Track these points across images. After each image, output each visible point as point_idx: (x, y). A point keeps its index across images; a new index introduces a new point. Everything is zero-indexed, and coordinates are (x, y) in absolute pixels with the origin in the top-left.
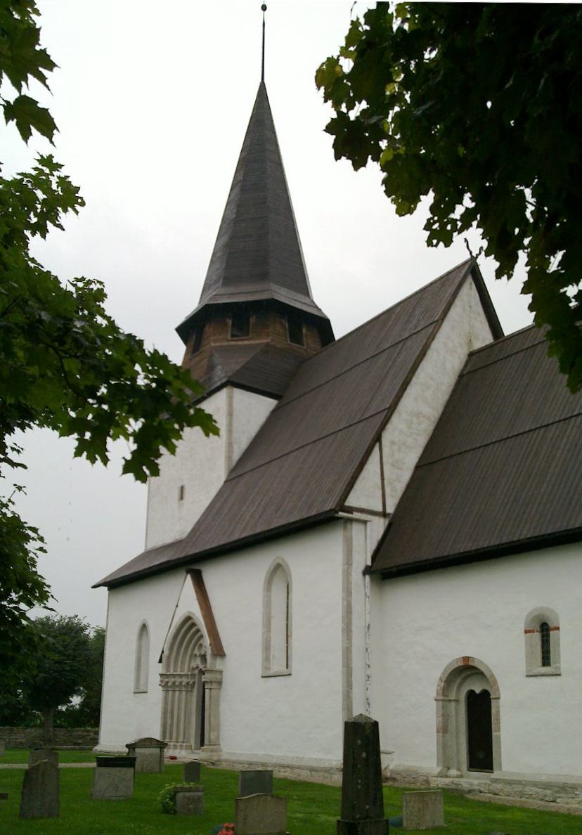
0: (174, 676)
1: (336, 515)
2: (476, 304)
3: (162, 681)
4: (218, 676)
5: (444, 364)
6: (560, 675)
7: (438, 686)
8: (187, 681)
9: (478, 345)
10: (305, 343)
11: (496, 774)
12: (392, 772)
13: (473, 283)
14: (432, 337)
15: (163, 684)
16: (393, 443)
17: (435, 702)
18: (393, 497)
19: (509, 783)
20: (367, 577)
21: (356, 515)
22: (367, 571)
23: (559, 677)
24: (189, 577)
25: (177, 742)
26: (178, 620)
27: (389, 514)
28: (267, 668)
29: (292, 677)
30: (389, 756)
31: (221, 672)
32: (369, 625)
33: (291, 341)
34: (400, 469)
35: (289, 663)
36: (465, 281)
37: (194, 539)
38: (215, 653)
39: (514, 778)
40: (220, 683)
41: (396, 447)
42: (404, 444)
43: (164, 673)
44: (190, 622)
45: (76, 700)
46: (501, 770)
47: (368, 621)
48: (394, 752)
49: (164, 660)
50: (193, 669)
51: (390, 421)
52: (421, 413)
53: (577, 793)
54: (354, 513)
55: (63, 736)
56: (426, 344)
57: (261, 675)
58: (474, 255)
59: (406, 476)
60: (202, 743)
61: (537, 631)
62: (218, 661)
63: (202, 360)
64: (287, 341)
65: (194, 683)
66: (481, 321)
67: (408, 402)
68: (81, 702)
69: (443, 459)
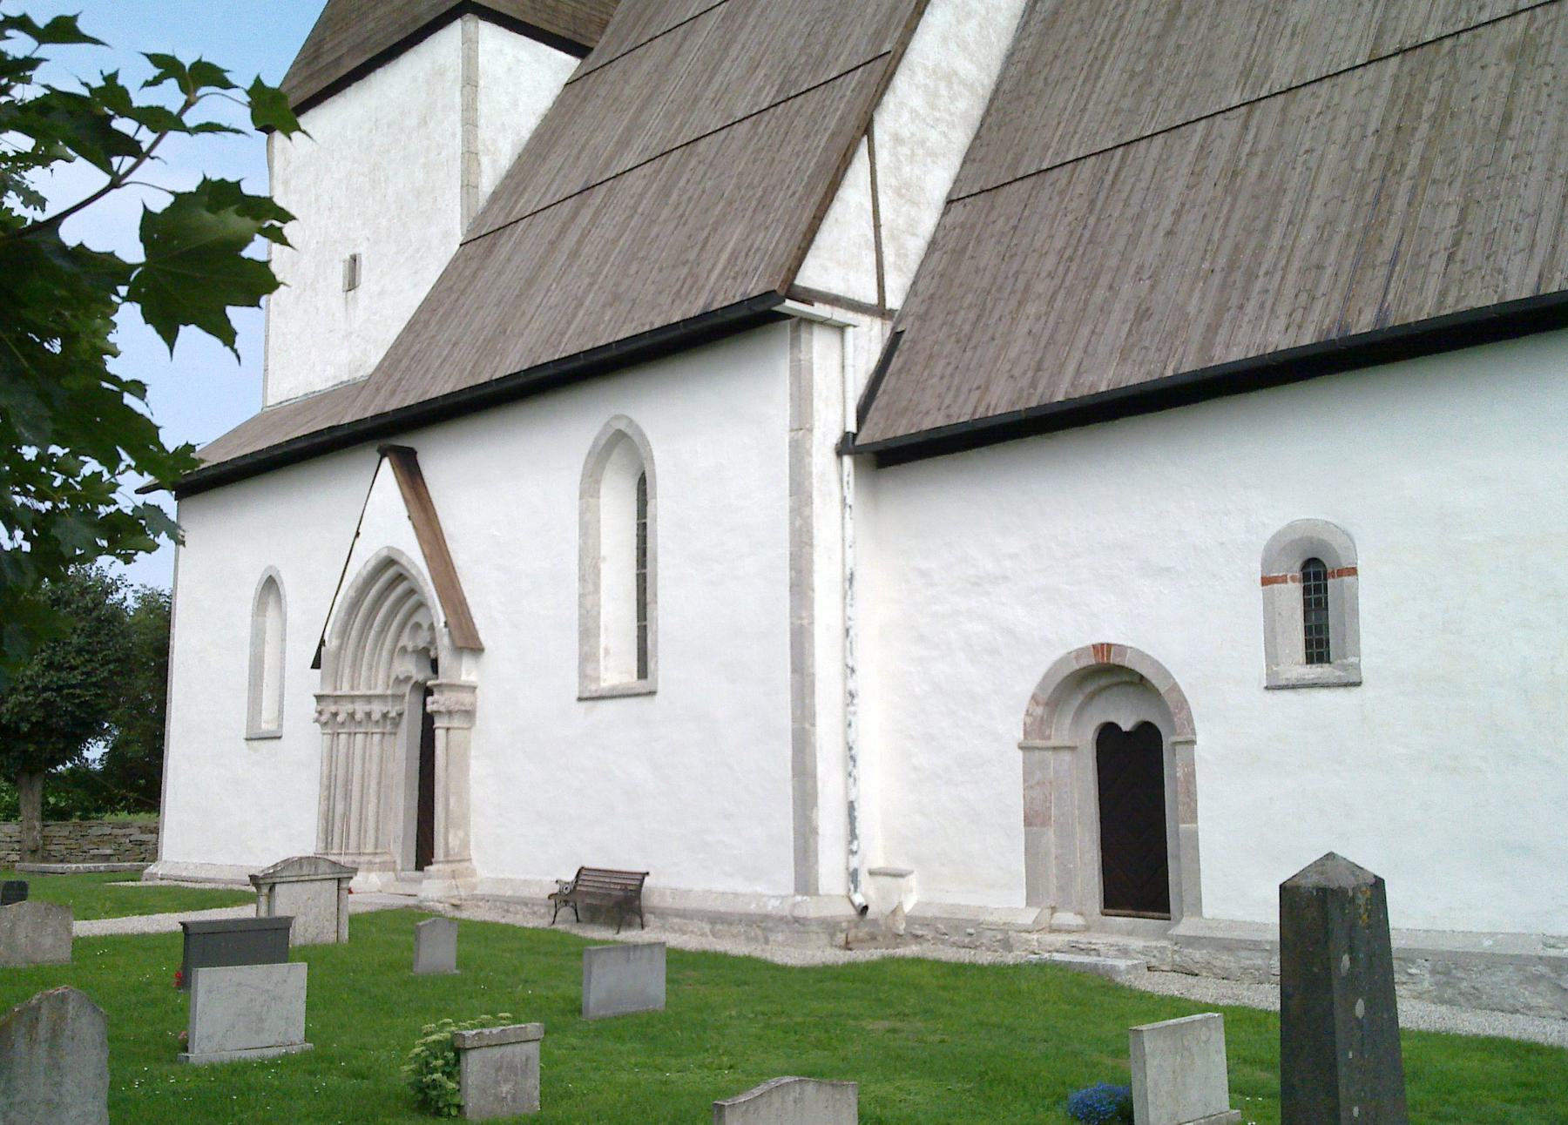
1: (777, 308)
4: (465, 697)
6: (1358, 684)
7: (1028, 714)
11: (1185, 926)
12: (911, 920)
15: (324, 718)
16: (898, 140)
17: (1020, 753)
18: (899, 269)
19: (1228, 946)
20: (847, 460)
21: (820, 310)
22: (846, 446)
23: (1355, 690)
24: (386, 463)
26: (360, 566)
27: (892, 311)
28: (583, 676)
29: (657, 697)
30: (900, 880)
31: (473, 689)
32: (852, 574)
37: (397, 375)
38: (460, 644)
39: (1236, 934)
40: (469, 714)
41: (904, 150)
44: (390, 573)
45: (95, 752)
46: (1200, 913)
47: (849, 564)
48: (911, 873)
50: (398, 681)
51: (891, 86)
52: (956, 73)
53: (1413, 971)
54: (816, 304)
55: (67, 838)
59: (928, 221)
61: (1293, 579)
62: (467, 662)
65: (400, 715)
67: (927, 45)
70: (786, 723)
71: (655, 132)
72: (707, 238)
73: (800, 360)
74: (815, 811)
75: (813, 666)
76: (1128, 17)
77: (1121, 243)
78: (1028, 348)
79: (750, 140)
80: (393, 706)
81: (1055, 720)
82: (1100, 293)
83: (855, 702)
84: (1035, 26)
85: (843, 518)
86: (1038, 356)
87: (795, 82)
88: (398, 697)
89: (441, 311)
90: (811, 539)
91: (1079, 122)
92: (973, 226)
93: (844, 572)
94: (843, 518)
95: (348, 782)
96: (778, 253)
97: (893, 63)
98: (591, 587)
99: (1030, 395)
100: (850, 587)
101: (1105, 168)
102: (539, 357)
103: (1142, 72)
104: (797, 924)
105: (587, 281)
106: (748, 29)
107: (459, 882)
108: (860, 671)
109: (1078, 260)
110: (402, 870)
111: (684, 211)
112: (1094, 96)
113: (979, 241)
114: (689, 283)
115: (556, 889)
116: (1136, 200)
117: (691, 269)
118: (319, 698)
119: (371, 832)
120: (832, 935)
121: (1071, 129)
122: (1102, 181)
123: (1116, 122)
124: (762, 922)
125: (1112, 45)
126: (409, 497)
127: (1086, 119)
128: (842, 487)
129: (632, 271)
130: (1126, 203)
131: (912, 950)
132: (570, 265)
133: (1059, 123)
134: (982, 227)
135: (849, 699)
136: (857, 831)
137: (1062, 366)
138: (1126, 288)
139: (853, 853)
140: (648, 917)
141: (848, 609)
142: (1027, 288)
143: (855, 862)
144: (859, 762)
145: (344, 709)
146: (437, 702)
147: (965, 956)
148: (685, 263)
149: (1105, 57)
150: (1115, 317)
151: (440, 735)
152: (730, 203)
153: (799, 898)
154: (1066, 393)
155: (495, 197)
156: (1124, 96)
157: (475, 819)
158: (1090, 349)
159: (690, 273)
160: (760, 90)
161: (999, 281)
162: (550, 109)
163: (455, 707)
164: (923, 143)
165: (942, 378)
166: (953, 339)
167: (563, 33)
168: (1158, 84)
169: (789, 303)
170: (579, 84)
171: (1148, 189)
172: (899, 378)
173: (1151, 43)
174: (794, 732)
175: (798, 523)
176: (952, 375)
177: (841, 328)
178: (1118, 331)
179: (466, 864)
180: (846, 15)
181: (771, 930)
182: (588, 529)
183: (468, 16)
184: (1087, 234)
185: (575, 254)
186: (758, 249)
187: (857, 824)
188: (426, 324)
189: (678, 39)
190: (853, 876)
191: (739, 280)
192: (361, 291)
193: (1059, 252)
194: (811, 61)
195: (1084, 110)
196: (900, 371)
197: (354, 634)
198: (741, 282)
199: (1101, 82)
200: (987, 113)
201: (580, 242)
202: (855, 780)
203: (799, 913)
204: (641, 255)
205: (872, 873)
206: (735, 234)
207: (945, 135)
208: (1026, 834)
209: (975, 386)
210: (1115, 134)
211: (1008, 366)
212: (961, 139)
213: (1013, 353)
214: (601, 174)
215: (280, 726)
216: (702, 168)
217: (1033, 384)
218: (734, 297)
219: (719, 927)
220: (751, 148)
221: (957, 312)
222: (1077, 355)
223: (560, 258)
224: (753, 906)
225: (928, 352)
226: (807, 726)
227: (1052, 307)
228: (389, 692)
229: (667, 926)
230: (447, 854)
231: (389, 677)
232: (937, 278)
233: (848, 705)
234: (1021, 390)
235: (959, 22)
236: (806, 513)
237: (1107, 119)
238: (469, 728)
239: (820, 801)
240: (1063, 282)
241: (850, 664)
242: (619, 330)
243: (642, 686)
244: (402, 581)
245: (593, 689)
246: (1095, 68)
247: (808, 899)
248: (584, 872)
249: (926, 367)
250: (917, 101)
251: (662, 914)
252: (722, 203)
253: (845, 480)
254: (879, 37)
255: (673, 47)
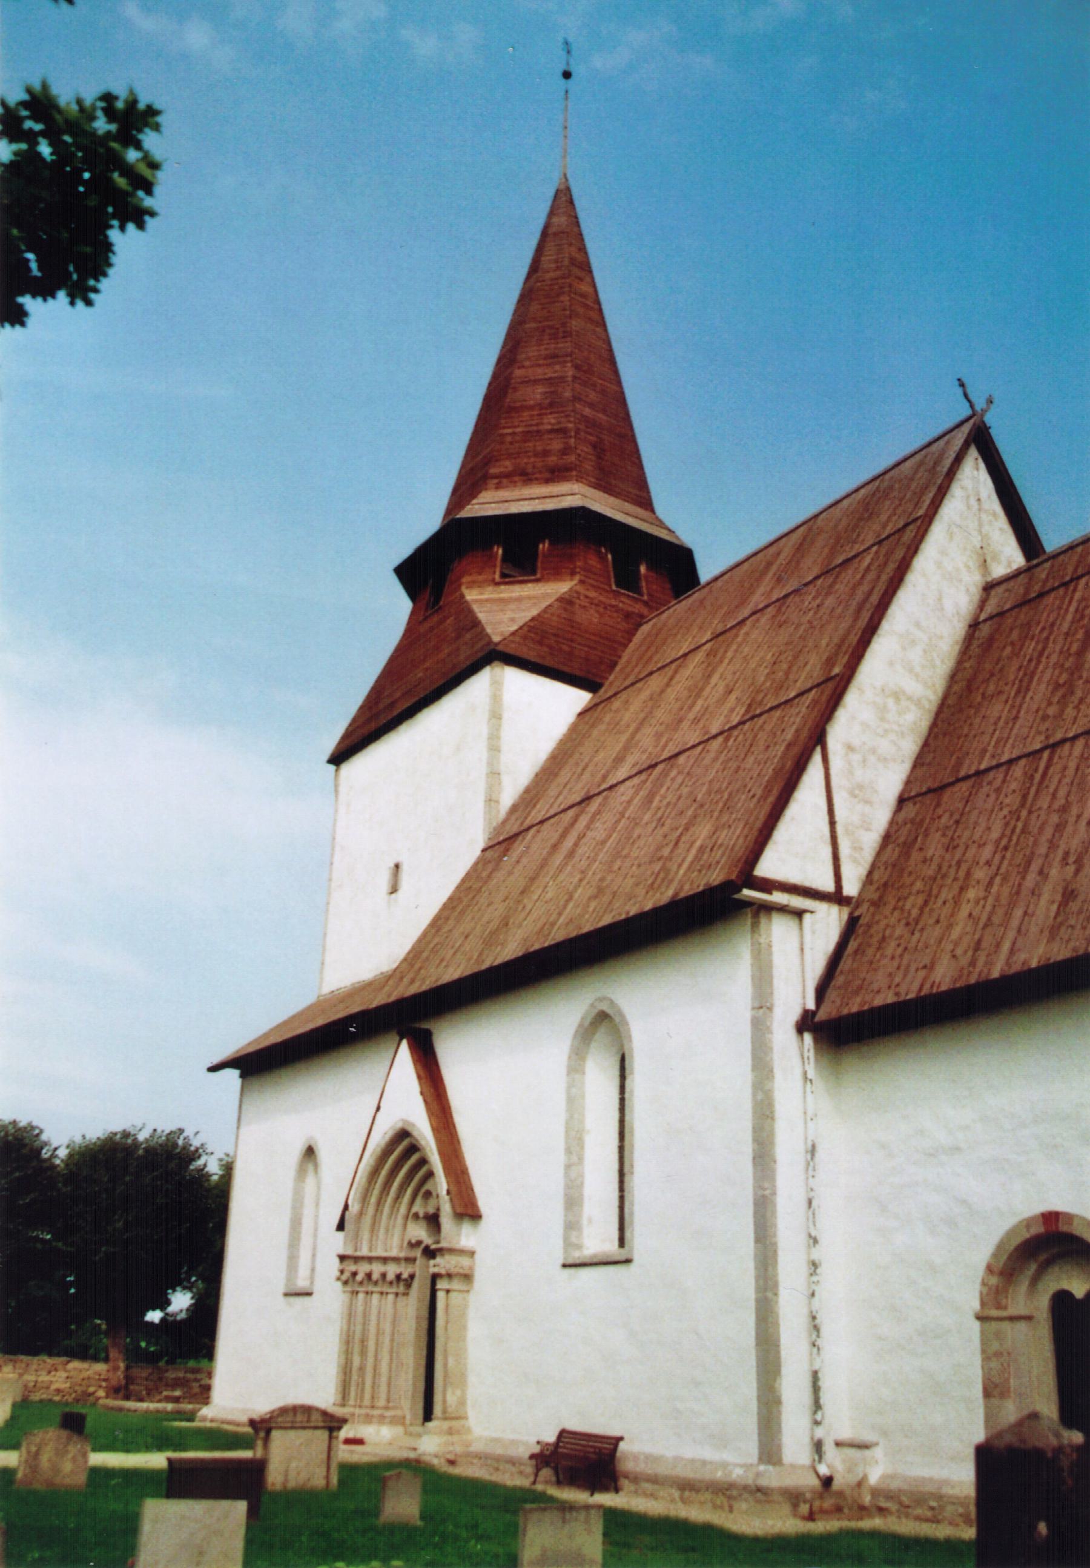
0: (370, 1259)
2: (989, 497)
3: (342, 1272)
4: (465, 1261)
5: (940, 599)
7: (984, 1283)
8: (398, 1271)
9: (999, 571)
10: (645, 591)
12: (875, 1492)
13: (980, 461)
14: (913, 548)
15: (344, 1277)
16: (850, 748)
18: (855, 861)
20: (808, 1037)
22: (806, 1023)
24: (404, 1044)
25: (373, 1407)
28: (568, 1244)
29: (633, 1267)
30: (867, 1452)
31: (472, 1254)
33: (617, 586)
34: (868, 802)
35: (628, 1234)
36: (966, 453)
37: (417, 966)
38: (459, 1210)
40: (467, 1277)
41: (856, 758)
42: (873, 751)
43: (349, 1252)
44: (405, 1143)
48: (877, 1444)
49: (348, 1225)
55: (147, 1379)
56: (904, 558)
57: (561, 1261)
58: (978, 408)
59: (881, 817)
60: (428, 1415)
62: (466, 1228)
63: (446, 618)
64: (610, 586)
66: (1001, 529)
68: (191, 1305)
69: (958, 780)
70: (748, 1291)
71: (647, 746)
72: (680, 837)
73: (760, 944)
74: (778, 1381)
75: (775, 1235)
76: (1052, 638)
77: (1049, 832)
78: (968, 929)
79: (722, 752)
80: (406, 1268)
81: (1010, 1291)
82: (1031, 878)
83: (818, 1271)
84: (975, 649)
85: (805, 1092)
86: (977, 937)
87: (761, 703)
88: (410, 1260)
89: (460, 907)
90: (772, 1112)
91: (1011, 729)
92: (922, 821)
93: (806, 1143)
94: (805, 1092)
95: (363, 1341)
96: (737, 848)
97: (843, 684)
98: (575, 1159)
99: (970, 973)
100: (812, 1159)
101: (1034, 767)
102: (533, 945)
103: (1065, 683)
104: (760, 1493)
105: (579, 876)
106: (726, 661)
107: (456, 1438)
108: (823, 1241)
109: (1011, 849)
110: (411, 1425)
111: (663, 815)
112: (1025, 706)
113: (926, 834)
114: (662, 875)
115: (537, 1449)
116: (1062, 793)
117: (664, 864)
118: (342, 1258)
119: (383, 1388)
120: (795, 1506)
121: (1005, 735)
122: (1032, 777)
123: (1043, 728)
124: (727, 1490)
125: (1039, 662)
126: (422, 1073)
127: (1017, 726)
128: (804, 1062)
129: (616, 867)
130: (1054, 796)
131: (876, 1523)
132: (566, 864)
133: (995, 730)
134: (930, 823)
135: (813, 1268)
136: (822, 1401)
137: (998, 945)
138: (1054, 872)
139: (817, 1423)
140: (624, 1483)
141: (811, 1179)
142: (968, 874)
143: (819, 1433)
144: (824, 1331)
145: (363, 1269)
146: (438, 1266)
147: (926, 1530)
148: (659, 859)
149: (1033, 673)
150: (1045, 897)
151: (441, 1295)
152: (702, 806)
153: (762, 1468)
154: (1002, 970)
155: (514, 809)
156: (1050, 704)
157: (472, 1379)
158: (1023, 928)
159: (663, 868)
160: (732, 710)
161: (944, 870)
162: (564, 735)
163: (453, 1271)
164: (873, 751)
165: (893, 958)
166: (903, 922)
167: (578, 673)
168: (1079, 694)
169: (747, 892)
170: (589, 713)
171: (1072, 783)
172: (854, 960)
173: (1071, 659)
174: (758, 1301)
175: (760, 1097)
176: (901, 956)
177: (799, 914)
178: (1048, 909)
179: (462, 1422)
180: (804, 646)
181: (735, 1498)
182: (574, 1103)
183: (496, 663)
184: (1020, 825)
185: (571, 854)
186: (721, 845)
187: (821, 1394)
188: (447, 919)
189: (670, 673)
190: (818, 1447)
191: (704, 872)
192: (400, 894)
193: (996, 841)
194: (775, 685)
195: (1016, 718)
196: (856, 952)
197: (373, 1200)
198: (706, 874)
199: (1030, 694)
200: (934, 725)
201: (576, 845)
202: (819, 1349)
203: (763, 1482)
204: (625, 852)
205: (838, 1444)
206: (702, 832)
207: (895, 744)
208: (986, 1407)
209: (921, 965)
210: (1042, 738)
211: (950, 947)
212: (910, 747)
213: (955, 934)
214: (599, 786)
215: (312, 1283)
216: (679, 779)
217: (973, 963)
218: (698, 887)
219: (687, 1494)
220: (722, 758)
221: (906, 898)
222: (1011, 934)
223: (558, 859)
224: (719, 1474)
225: (881, 935)
226: (769, 1295)
227: (990, 892)
228: (402, 1255)
229: (640, 1491)
230: (444, 1411)
231: (403, 1240)
232: (889, 869)
233: (811, 1275)
234: (962, 969)
235: (904, 649)
236: (767, 1088)
237: (1035, 725)
238: (468, 1291)
239: (784, 1371)
240: (998, 869)
241: (813, 1234)
242: (600, 920)
243: (621, 1254)
244: (414, 1153)
245: (576, 1256)
246: (1025, 684)
247: (771, 1468)
248: (565, 1435)
249: (878, 949)
250: (867, 715)
251: (636, 1479)
252: (695, 805)
253: (806, 1055)
254: (830, 662)
255: (666, 680)
